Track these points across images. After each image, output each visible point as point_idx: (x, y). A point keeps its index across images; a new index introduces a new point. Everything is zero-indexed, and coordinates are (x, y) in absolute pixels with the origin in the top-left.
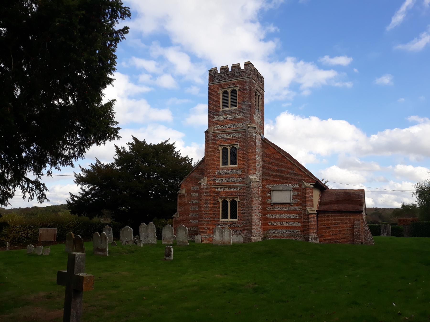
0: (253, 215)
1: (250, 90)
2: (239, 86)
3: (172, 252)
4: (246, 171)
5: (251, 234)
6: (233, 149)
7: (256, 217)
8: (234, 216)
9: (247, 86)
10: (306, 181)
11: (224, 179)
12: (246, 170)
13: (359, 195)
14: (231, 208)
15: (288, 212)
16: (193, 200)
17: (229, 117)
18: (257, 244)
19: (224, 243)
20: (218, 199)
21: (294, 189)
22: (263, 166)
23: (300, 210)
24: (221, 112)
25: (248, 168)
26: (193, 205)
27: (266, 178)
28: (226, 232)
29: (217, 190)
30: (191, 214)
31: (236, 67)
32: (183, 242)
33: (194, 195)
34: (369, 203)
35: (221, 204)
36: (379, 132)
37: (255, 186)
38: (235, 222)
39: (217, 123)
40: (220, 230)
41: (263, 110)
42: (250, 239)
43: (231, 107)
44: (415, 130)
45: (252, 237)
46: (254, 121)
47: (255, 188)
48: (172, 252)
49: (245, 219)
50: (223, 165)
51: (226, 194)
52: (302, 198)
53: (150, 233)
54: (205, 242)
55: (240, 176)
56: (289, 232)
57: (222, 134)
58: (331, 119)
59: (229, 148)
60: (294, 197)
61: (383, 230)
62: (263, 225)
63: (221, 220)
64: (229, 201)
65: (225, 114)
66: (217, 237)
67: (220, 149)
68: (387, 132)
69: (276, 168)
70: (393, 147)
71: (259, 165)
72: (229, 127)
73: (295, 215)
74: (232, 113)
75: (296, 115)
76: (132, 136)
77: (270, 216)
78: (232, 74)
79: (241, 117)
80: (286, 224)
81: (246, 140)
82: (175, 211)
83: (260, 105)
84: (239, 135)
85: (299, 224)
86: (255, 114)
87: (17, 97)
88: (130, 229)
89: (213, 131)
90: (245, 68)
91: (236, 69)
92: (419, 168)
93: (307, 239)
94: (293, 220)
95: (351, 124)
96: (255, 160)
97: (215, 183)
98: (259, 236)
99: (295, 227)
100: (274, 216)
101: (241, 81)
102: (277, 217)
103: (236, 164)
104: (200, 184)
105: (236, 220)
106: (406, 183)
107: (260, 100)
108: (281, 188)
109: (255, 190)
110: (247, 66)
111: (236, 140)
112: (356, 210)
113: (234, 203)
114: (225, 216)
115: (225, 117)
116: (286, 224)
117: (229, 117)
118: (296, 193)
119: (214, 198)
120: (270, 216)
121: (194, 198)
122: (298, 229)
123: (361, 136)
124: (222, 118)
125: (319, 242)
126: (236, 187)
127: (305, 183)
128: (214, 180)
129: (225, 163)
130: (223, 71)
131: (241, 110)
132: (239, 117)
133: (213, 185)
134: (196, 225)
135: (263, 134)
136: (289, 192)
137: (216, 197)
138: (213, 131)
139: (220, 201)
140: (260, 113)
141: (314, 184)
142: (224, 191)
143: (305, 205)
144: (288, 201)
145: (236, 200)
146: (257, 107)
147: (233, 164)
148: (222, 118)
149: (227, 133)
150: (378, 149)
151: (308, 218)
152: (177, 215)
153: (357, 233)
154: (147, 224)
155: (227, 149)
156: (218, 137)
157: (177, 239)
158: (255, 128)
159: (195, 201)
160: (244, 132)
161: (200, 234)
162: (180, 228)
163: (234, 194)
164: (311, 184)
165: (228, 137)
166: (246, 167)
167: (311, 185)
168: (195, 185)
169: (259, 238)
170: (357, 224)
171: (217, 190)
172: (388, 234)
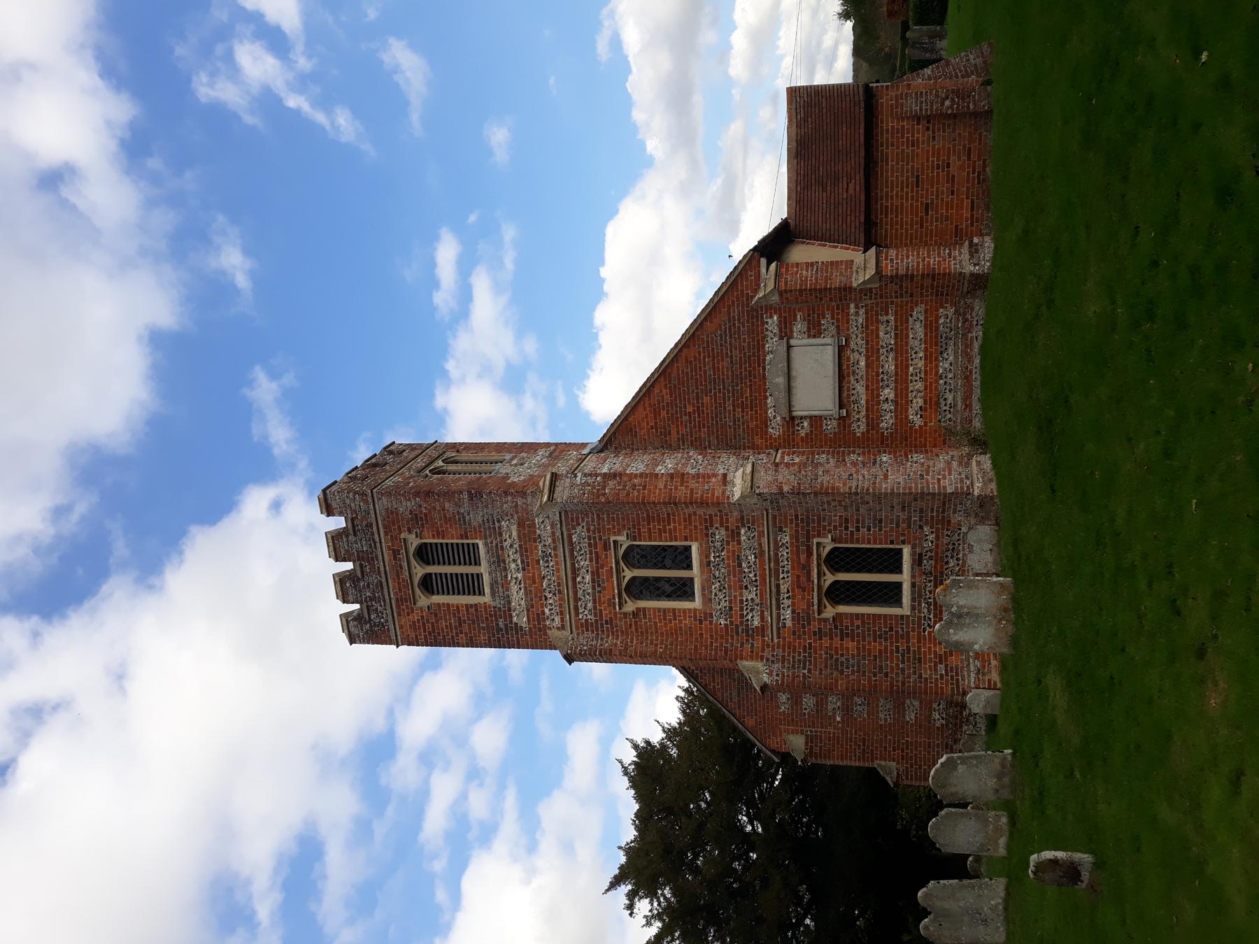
0: (886, 487)
1: (417, 494)
2: (403, 536)
3: (1060, 855)
4: (712, 513)
5: (962, 495)
6: (633, 557)
7: (894, 474)
8: (892, 561)
9: (405, 506)
10: (756, 291)
11: (750, 595)
12: (711, 511)
13: (808, 107)
14: (860, 568)
15: (873, 353)
16: (830, 707)
17: (514, 571)
18: (1002, 473)
19: (1006, 610)
20: (825, 620)
21: (785, 333)
22: (700, 446)
23: (862, 311)
24: (498, 603)
25: (703, 503)
26: (847, 710)
27: (743, 435)
28: (961, 599)
29: (789, 623)
30: (882, 716)
31: (338, 545)
32: (999, 776)
33: (809, 701)
34: (837, 67)
35: (843, 609)
36: (639, 137)
37: (770, 478)
38: (913, 554)
39: (537, 618)
40: (950, 624)
41: (500, 447)
42: (983, 501)
43: (477, 563)
44: (632, 38)
45: (976, 492)
46: (533, 481)
47: (780, 478)
48: (1060, 855)
49: (903, 516)
51: (804, 590)
53: (962, 904)
54: (995, 677)
55: (735, 535)
56: (950, 351)
57: (577, 600)
58: (601, 269)
59: (628, 574)
60: (814, 330)
61: (926, 50)
62: (920, 447)
63: (905, 610)
64: (830, 578)
66: (980, 636)
67: (630, 606)
68: (638, 116)
69: (706, 400)
70: (678, 95)
71: (695, 462)
72: (550, 574)
73: (882, 328)
74: (499, 562)
75: (589, 366)
76: (607, 890)
77: (887, 421)
78: (364, 559)
79: (514, 529)
81: (602, 509)
82: (872, 775)
83: (480, 456)
84: (580, 534)
85: (918, 312)
86: (507, 476)
87: (667, 892)
88: (931, 892)
89: (567, 633)
90: (341, 514)
91: (343, 545)
92: (738, 16)
93: (978, 283)
95: (617, 212)
96: (672, 476)
97: (762, 630)
98: (968, 465)
100: (885, 406)
101: (385, 527)
102: (892, 396)
103: (688, 549)
104: (764, 687)
105: (906, 552)
106: (781, 43)
107: (464, 456)
108: (781, 380)
109: (787, 479)
110: (334, 505)
111: (599, 547)
112: (861, 110)
113: (837, 560)
114: (891, 594)
115: (514, 588)
117: (514, 571)
118: (799, 326)
119: (820, 634)
120: (887, 421)
121: (820, 704)
122: (937, 318)
123: (652, 183)
124: (517, 597)
125: (987, 239)
126: (777, 548)
127: (761, 294)
128: (750, 633)
129: (683, 589)
130: (351, 592)
131: (492, 530)
132: (515, 534)
133: (771, 636)
135: (584, 445)
136: (795, 353)
137: (815, 626)
138: (567, 633)
140: (508, 457)
141: (763, 261)
142: (794, 597)
143: (846, 292)
146: (485, 467)
147: (689, 557)
148: (517, 597)
149: (574, 579)
150: (683, 137)
151: (896, 278)
152: (889, 769)
153: (947, 103)
154: (926, 913)
155: (633, 579)
156: (586, 615)
157: (990, 796)
158: (555, 477)
159: (834, 702)
160: (569, 517)
161: (965, 694)
162: (944, 786)
163: (803, 557)
164: (763, 270)
165: (588, 578)
166: (700, 511)
167: (768, 272)
169: (978, 463)
170: (913, 106)
171: (789, 623)
172: (941, 37)
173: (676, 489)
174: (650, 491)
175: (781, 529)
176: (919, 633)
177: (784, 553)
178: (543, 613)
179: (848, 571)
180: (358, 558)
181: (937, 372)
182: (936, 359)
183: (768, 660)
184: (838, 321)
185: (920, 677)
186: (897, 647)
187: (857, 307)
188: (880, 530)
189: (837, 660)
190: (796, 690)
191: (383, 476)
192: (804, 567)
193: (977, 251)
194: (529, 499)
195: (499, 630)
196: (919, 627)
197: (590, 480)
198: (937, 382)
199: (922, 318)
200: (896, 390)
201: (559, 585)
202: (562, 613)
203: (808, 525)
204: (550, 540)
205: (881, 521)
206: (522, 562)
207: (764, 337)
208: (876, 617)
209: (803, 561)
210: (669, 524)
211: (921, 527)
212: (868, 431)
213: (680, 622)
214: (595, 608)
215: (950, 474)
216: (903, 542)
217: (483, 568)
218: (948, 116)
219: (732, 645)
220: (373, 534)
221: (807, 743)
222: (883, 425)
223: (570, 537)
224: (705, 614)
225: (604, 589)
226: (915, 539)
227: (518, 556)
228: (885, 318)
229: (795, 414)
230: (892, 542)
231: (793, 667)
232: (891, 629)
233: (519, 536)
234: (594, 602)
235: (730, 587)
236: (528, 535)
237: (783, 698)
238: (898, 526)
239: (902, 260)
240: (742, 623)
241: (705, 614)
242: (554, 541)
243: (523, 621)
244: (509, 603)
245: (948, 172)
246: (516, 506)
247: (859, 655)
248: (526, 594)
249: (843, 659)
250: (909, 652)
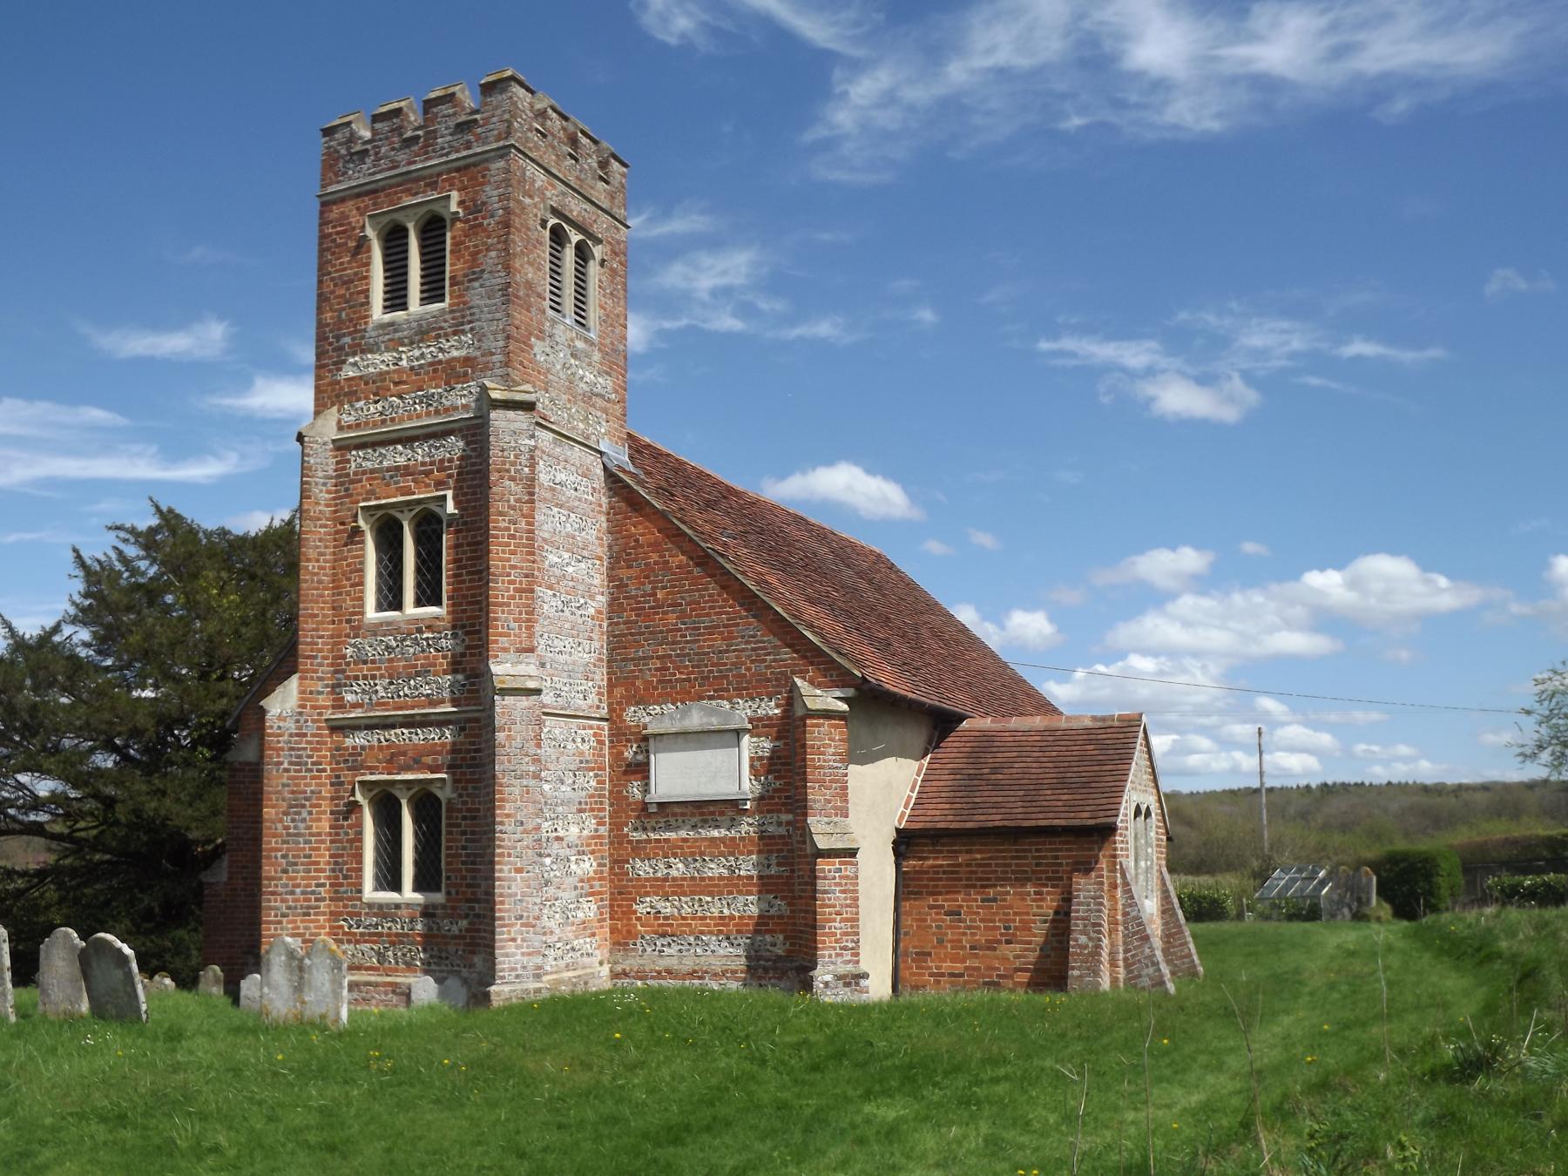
23: (782, 831)
51: (388, 762)
65: (394, 344)
69: (672, 618)
77: (643, 868)
79: (463, 353)
102: (674, 873)
112: (1085, 819)
115: (387, 357)
124: (378, 362)
129: (391, 597)
131: (460, 322)
132: (455, 353)
137: (346, 776)
141: (850, 692)
144: (724, 788)
145: (439, 794)
148: (378, 362)
163: (429, 760)
165: (401, 461)
173: (510, 582)
174: (508, 545)
175: (463, 729)
176: (341, 914)
178: (358, 400)
181: (702, 933)
182: (720, 932)
183: (300, 714)
184: (772, 798)
185: (284, 915)
186: (323, 885)
187: (788, 823)
188: (464, 863)
189: (303, 806)
191: (549, 159)
192: (416, 761)
193: (847, 985)
194: (499, 372)
195: (338, 338)
196: (349, 914)
197: (523, 459)
198: (692, 933)
199: (772, 912)
200: (684, 879)
201: (393, 420)
203: (470, 766)
204: (447, 403)
205: (473, 863)
206: (421, 366)
208: (359, 857)
209: (424, 759)
210: (469, 573)
211: (467, 916)
212: (630, 842)
213: (348, 593)
214: (364, 473)
215: (523, 954)
216: (448, 893)
219: (321, 665)
220: (458, 151)
221: (249, 764)
222: (639, 863)
224: (359, 628)
225: (388, 485)
226: (453, 908)
228: (774, 861)
229: (651, 741)
230: (448, 878)
231: (292, 749)
232: (346, 877)
233: (454, 359)
234: (373, 471)
235: (391, 661)
236: (451, 373)
238: (469, 886)
239: (837, 885)
240: (348, 678)
241: (359, 628)
242: (446, 410)
243: (349, 372)
244: (371, 352)
245: (999, 942)
246: (492, 354)
247: (312, 835)
248: (381, 374)
249: (305, 815)
250: (317, 900)
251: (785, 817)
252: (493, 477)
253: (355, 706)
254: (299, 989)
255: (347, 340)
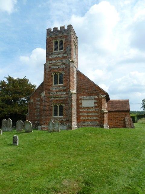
8: (61, 115)
10: (101, 95)
15: (92, 112)
17: (58, 56)
21: (95, 99)
22: (77, 86)
26: (37, 108)
29: (51, 99)
31: (56, 29)
33: (38, 103)
39: (51, 59)
43: (60, 50)
50: (54, 84)
52: (99, 104)
55: (64, 91)
59: (58, 74)
60: (95, 103)
64: (58, 105)
67: (53, 74)
71: (75, 86)
72: (58, 61)
74: (60, 53)
77: (81, 114)
79: (65, 56)
80: (90, 118)
84: (64, 66)
85: (98, 118)
94: (94, 116)
97: (49, 95)
99: (95, 120)
105: (62, 117)
107: (76, 49)
111: (62, 69)
114: (56, 114)
115: (56, 56)
116: (90, 118)
117: (58, 56)
118: (96, 101)
119: (49, 104)
120: (81, 114)
121: (38, 104)
128: (49, 93)
129: (56, 83)
133: (49, 96)
134: (39, 120)
136: (92, 100)
139: (53, 105)
147: (61, 84)
148: (54, 56)
149: (57, 65)
151: (103, 115)
156: (52, 67)
159: (38, 106)
163: (61, 101)
168: (38, 97)
171: (51, 99)
177: (62, 98)
179: (59, 108)
180: (61, 31)
190: (40, 100)
202: (52, 63)
207: (94, 96)
217: (59, 51)
218: (125, 122)
223: (64, 65)
227: (61, 56)
237: (38, 99)
243: (50, 57)
251: (98, 109)
252: (70, 70)
253: (51, 95)
254: (54, 127)
255: (50, 54)
